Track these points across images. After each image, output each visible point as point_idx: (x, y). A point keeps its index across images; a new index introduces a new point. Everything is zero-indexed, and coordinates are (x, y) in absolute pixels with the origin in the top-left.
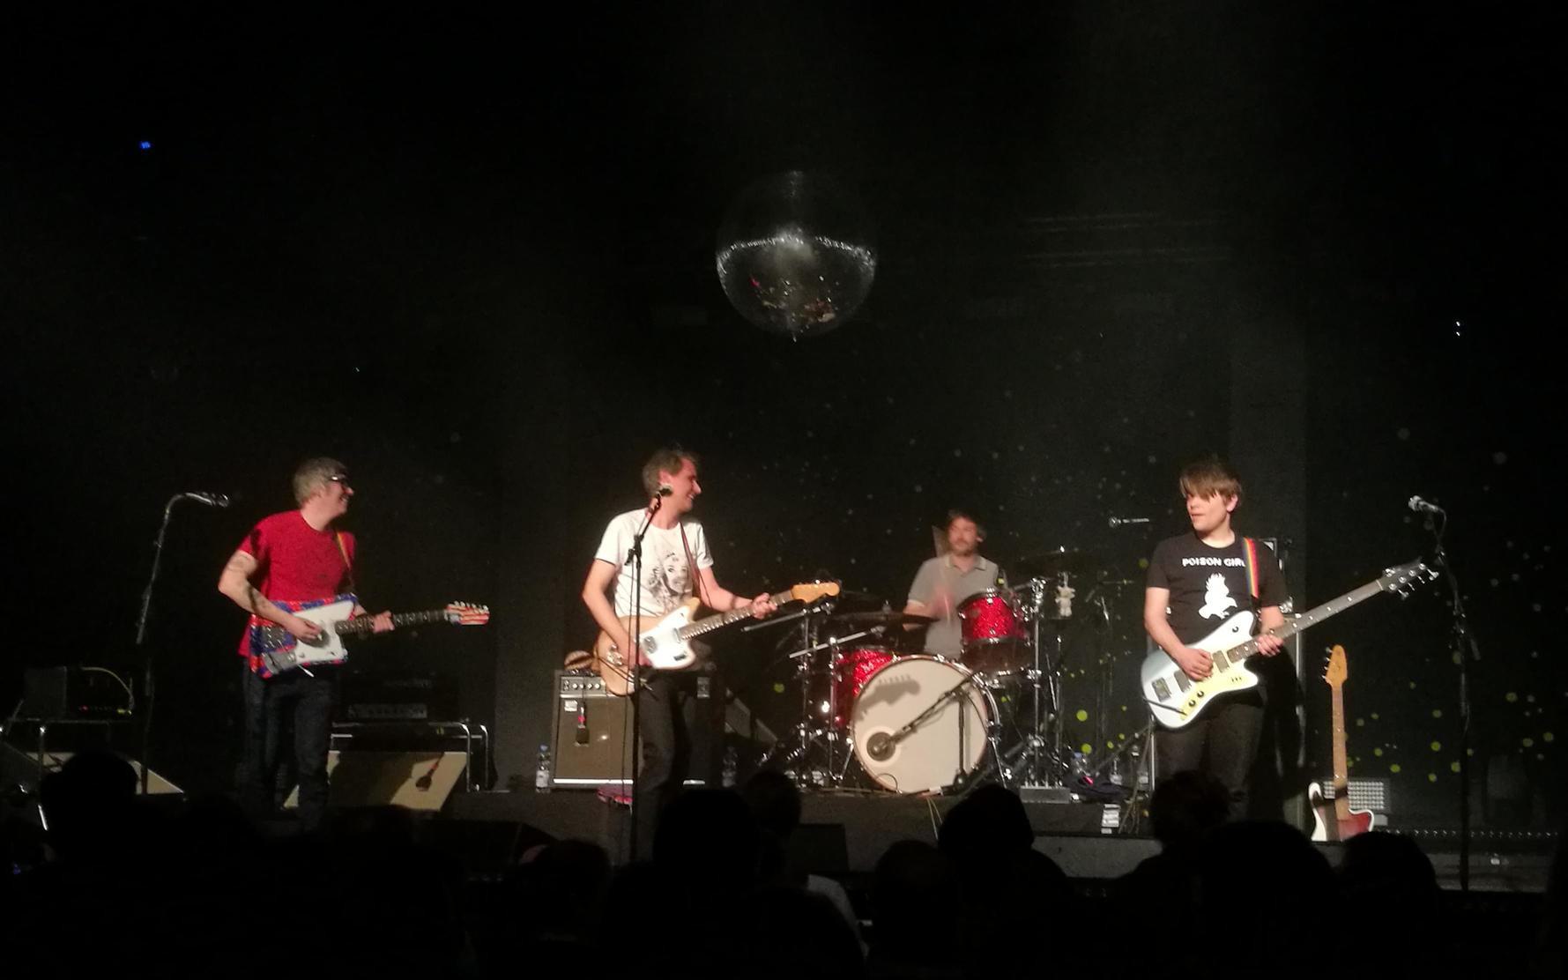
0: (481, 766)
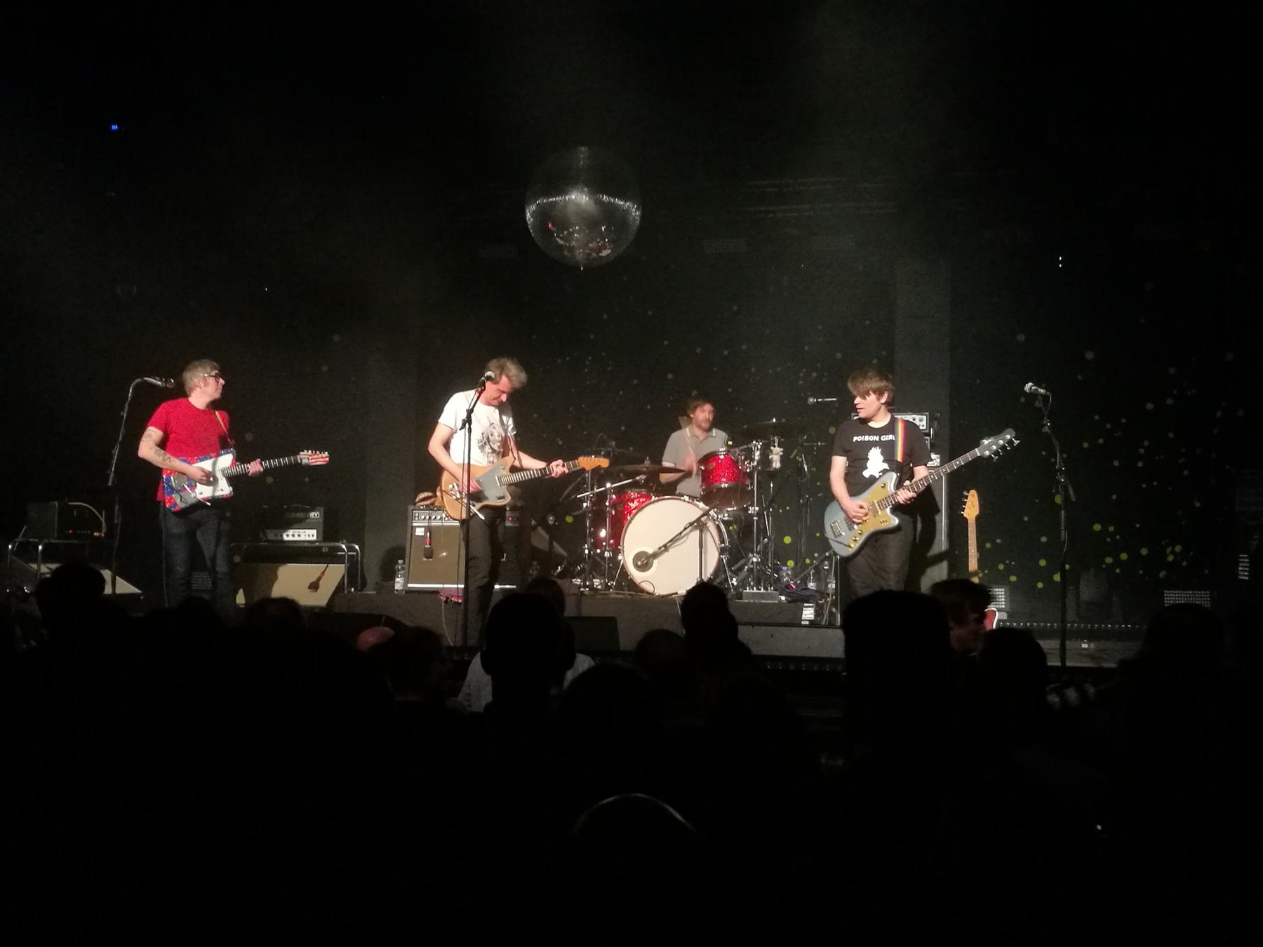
0: (355, 575)
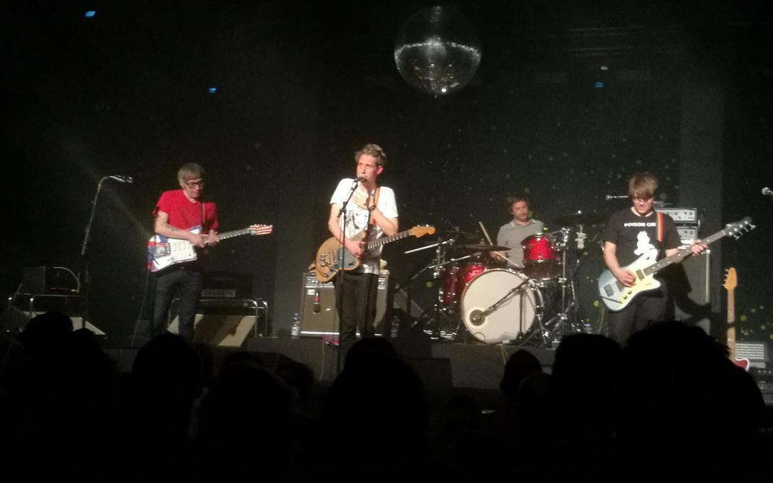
0: (264, 323)
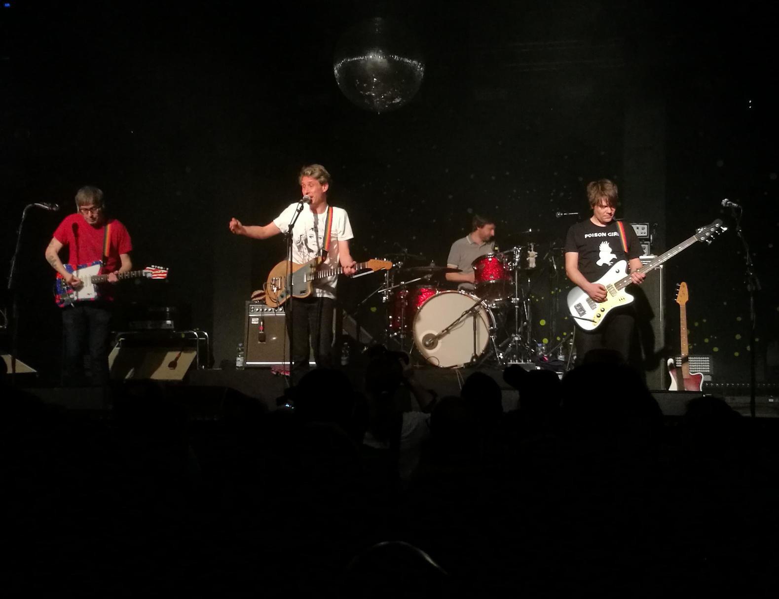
0: (205, 355)
